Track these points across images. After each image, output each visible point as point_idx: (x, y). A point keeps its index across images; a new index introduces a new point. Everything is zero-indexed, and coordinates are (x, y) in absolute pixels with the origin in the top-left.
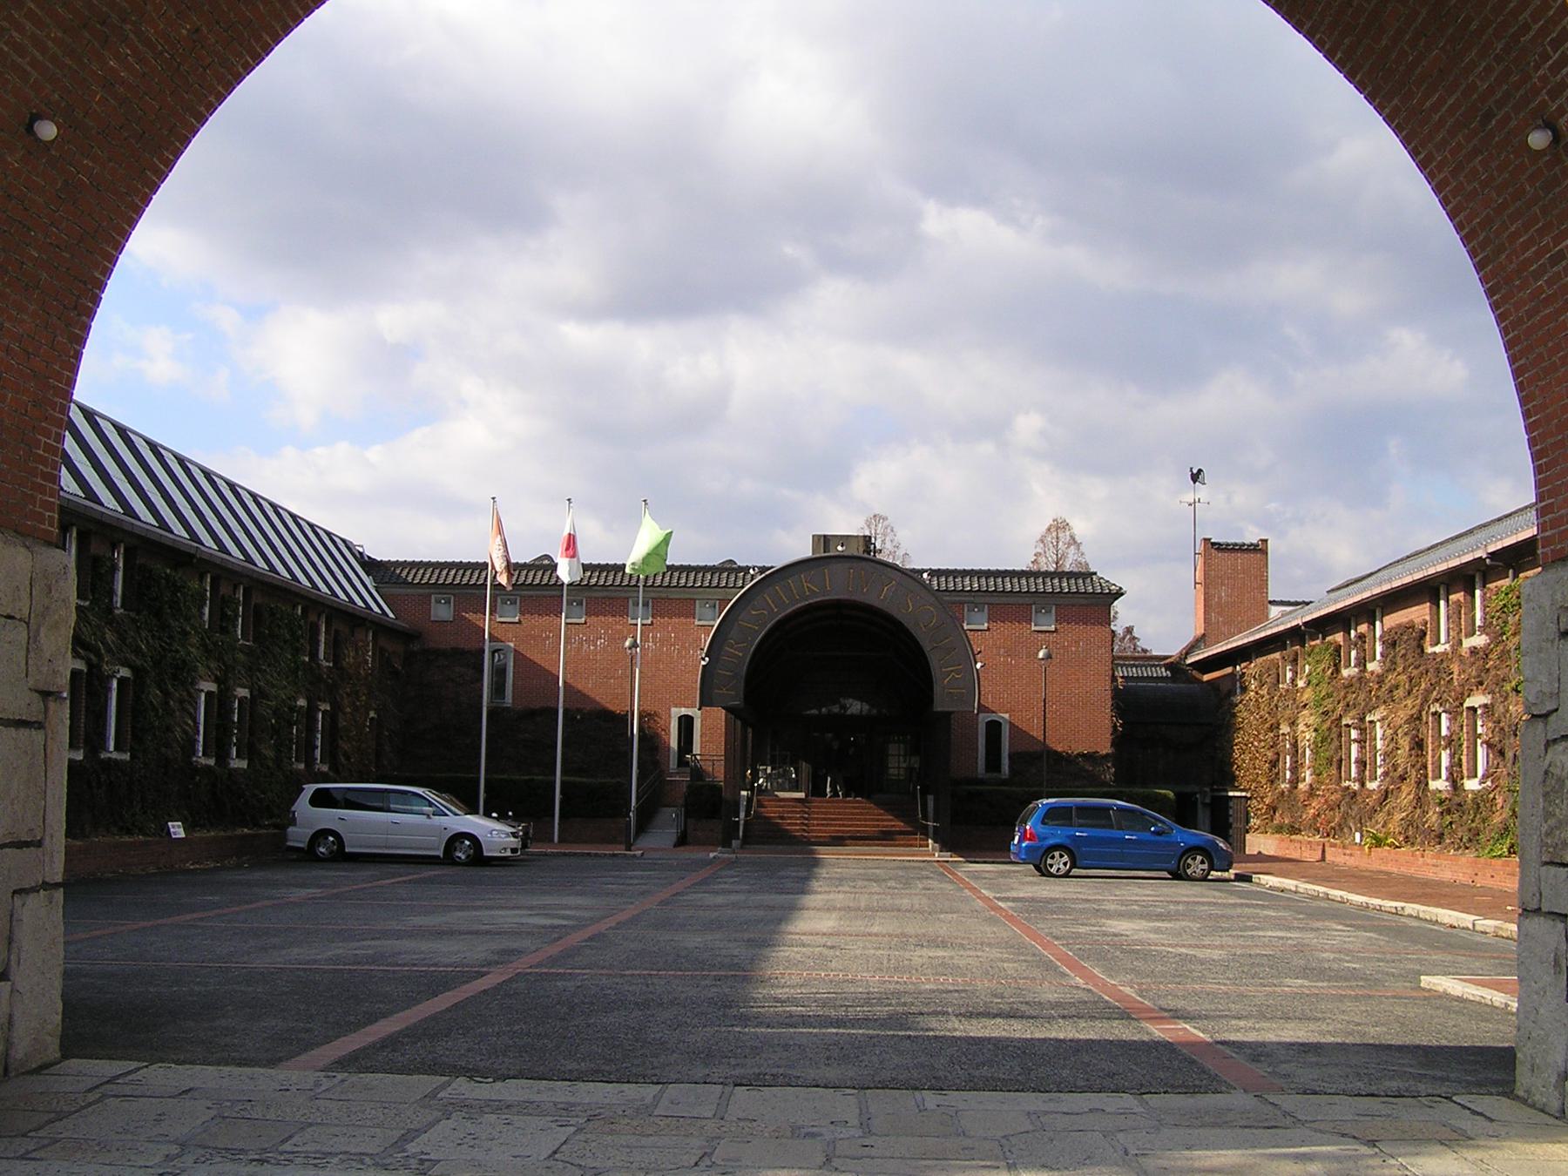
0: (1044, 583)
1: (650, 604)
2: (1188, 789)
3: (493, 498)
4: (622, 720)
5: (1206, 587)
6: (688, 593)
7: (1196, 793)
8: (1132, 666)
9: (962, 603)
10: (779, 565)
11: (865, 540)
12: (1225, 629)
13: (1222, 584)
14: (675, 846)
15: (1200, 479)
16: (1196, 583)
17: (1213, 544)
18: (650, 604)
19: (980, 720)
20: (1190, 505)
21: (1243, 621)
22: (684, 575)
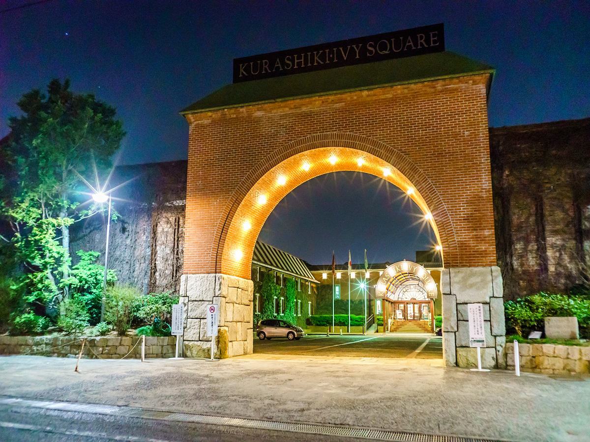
14: (375, 333)
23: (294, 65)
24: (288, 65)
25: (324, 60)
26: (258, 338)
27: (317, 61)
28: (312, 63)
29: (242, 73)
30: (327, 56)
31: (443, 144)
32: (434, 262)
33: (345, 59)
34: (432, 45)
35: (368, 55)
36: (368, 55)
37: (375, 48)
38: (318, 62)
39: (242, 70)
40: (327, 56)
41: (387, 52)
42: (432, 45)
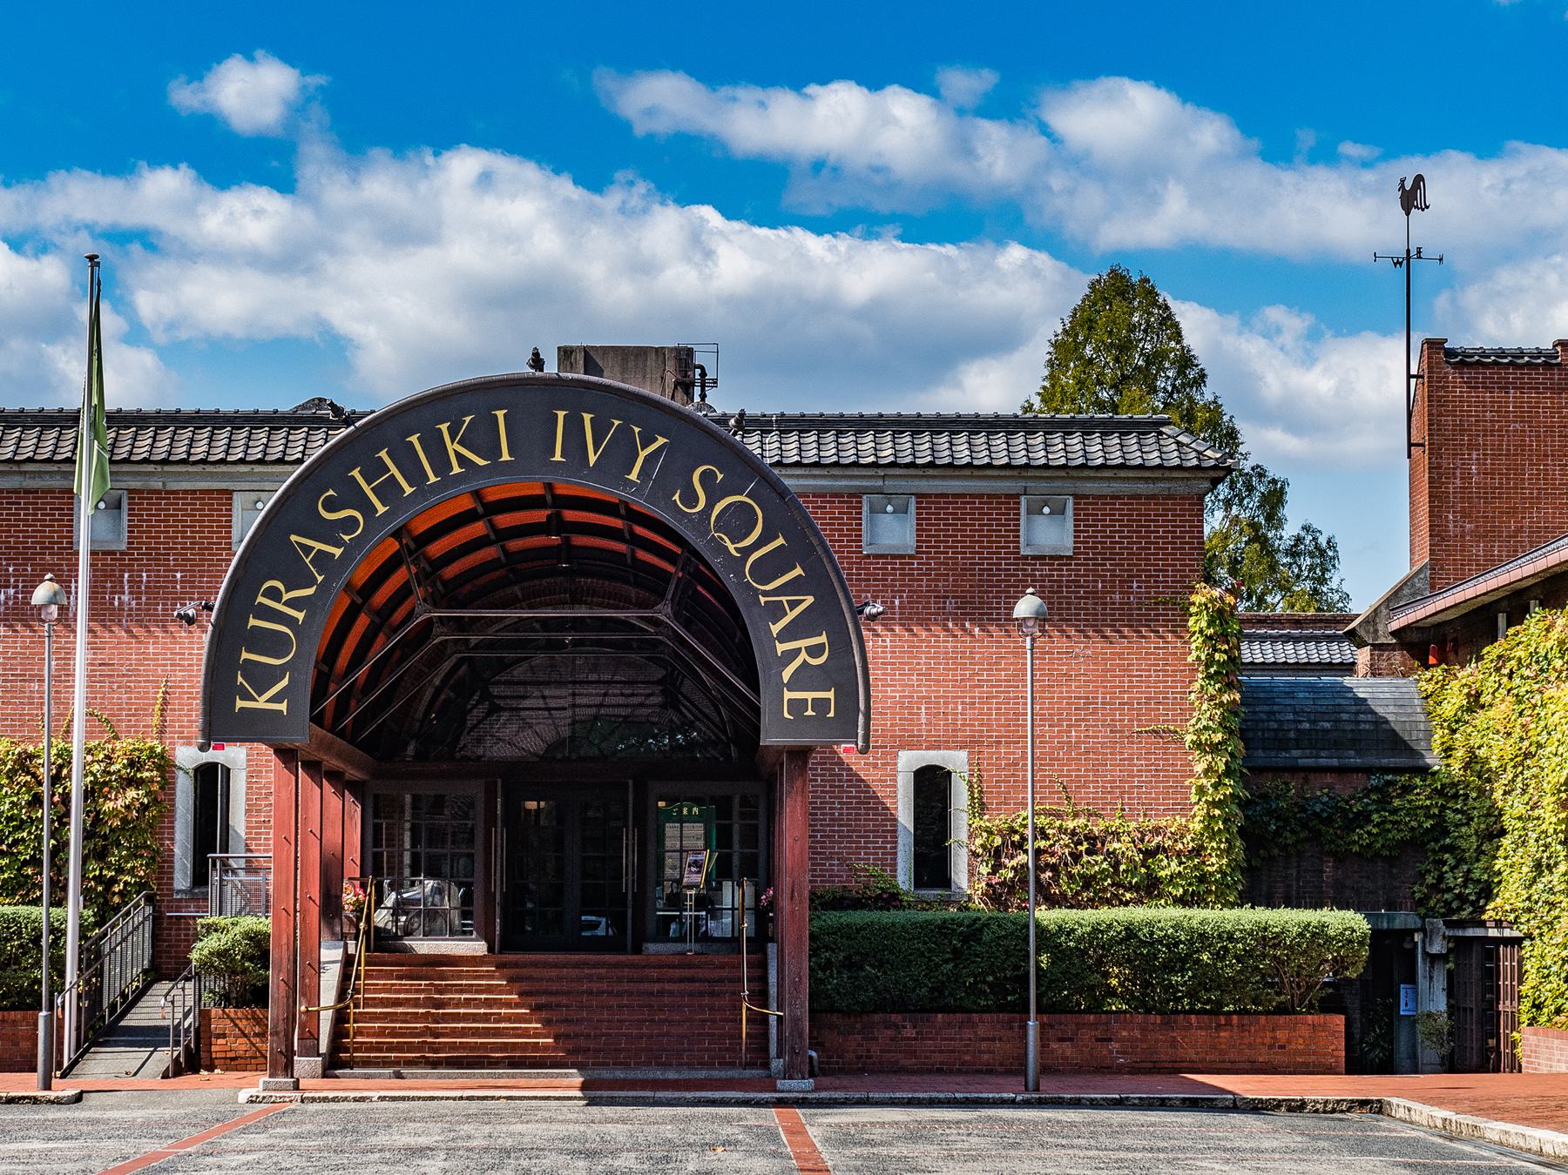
0: (1047, 446)
1: (125, 506)
2: (1404, 919)
3: (92, 258)
4: (1338, 909)
5: (1435, 451)
6: (212, 475)
7: (1411, 932)
8: (1287, 639)
9: (857, 495)
10: (381, 407)
11: (678, 359)
12: (1479, 550)
13: (1470, 447)
14: (165, 1076)
15: (1417, 202)
16: (1410, 445)
17: (1451, 353)
18: (125, 506)
19: (900, 767)
20: (1398, 263)
21: (1519, 530)
22: (206, 433)
23: (367, 509)
24: (350, 524)
25: (493, 451)
26: (475, 933)
27: (457, 454)
28: (441, 464)
29: (276, 699)
30: (630, 809)
31: (1534, 458)
32: (757, 818)
33: (810, 600)
34: (788, 695)
35: (720, 477)
36: (331, 492)
37: (1238, 681)
38: (276, 699)
39: (261, 703)
40: (630, 809)
41: (731, 547)
42: (788, 695)
